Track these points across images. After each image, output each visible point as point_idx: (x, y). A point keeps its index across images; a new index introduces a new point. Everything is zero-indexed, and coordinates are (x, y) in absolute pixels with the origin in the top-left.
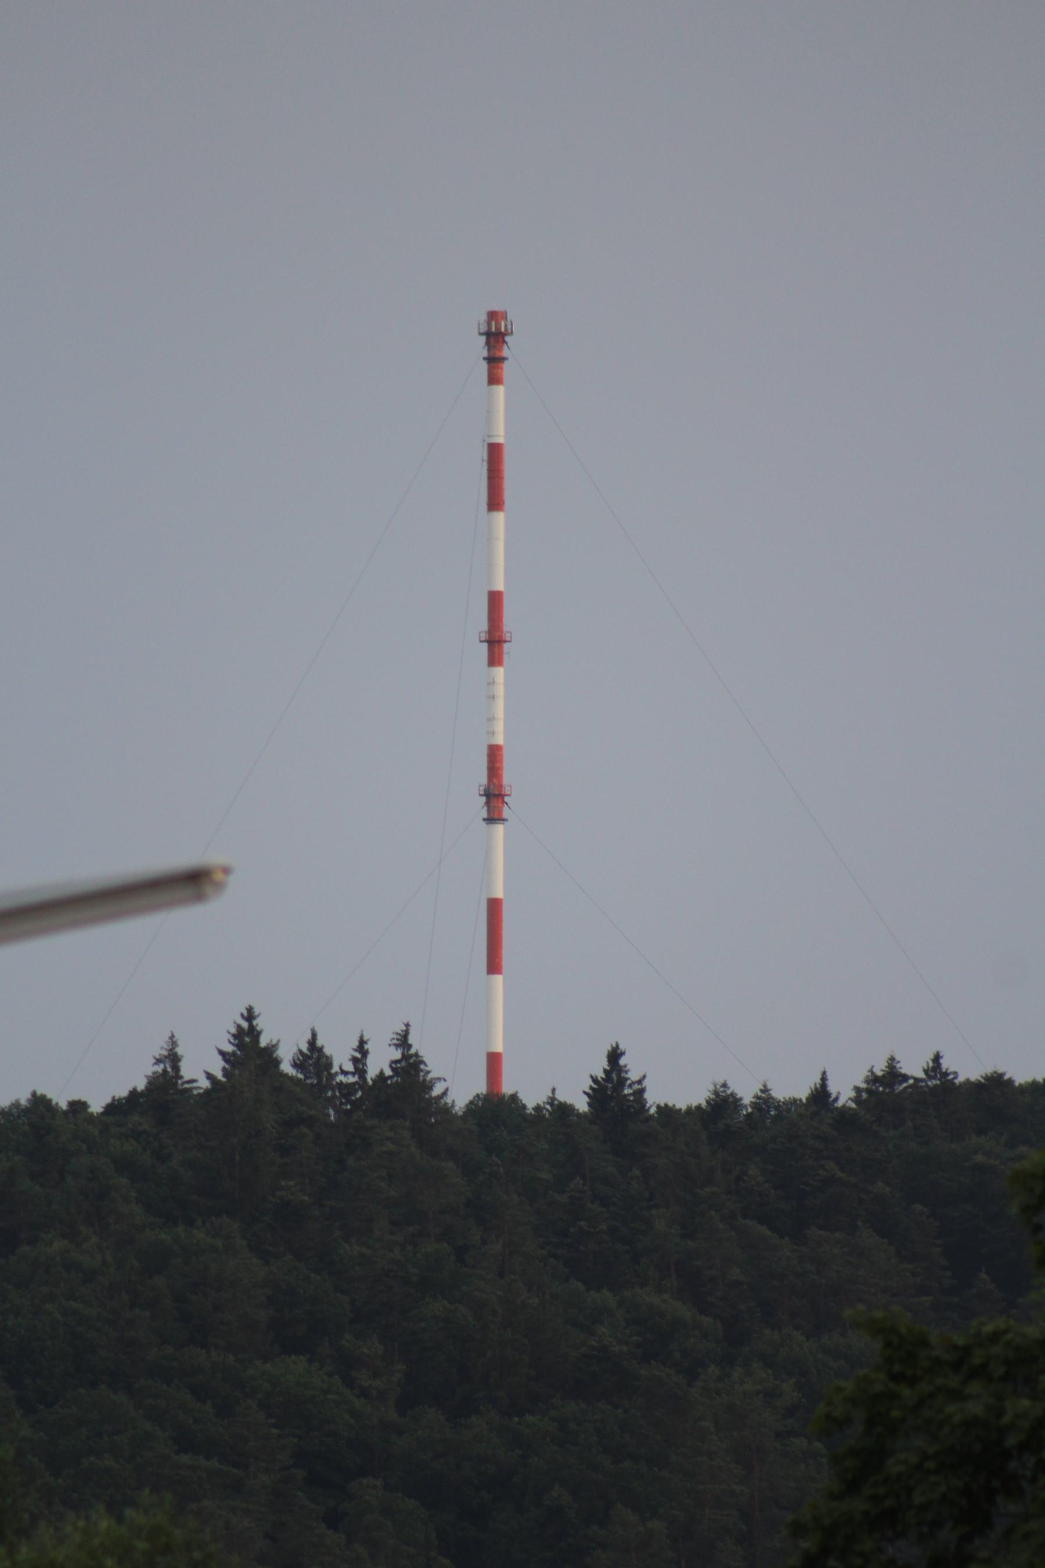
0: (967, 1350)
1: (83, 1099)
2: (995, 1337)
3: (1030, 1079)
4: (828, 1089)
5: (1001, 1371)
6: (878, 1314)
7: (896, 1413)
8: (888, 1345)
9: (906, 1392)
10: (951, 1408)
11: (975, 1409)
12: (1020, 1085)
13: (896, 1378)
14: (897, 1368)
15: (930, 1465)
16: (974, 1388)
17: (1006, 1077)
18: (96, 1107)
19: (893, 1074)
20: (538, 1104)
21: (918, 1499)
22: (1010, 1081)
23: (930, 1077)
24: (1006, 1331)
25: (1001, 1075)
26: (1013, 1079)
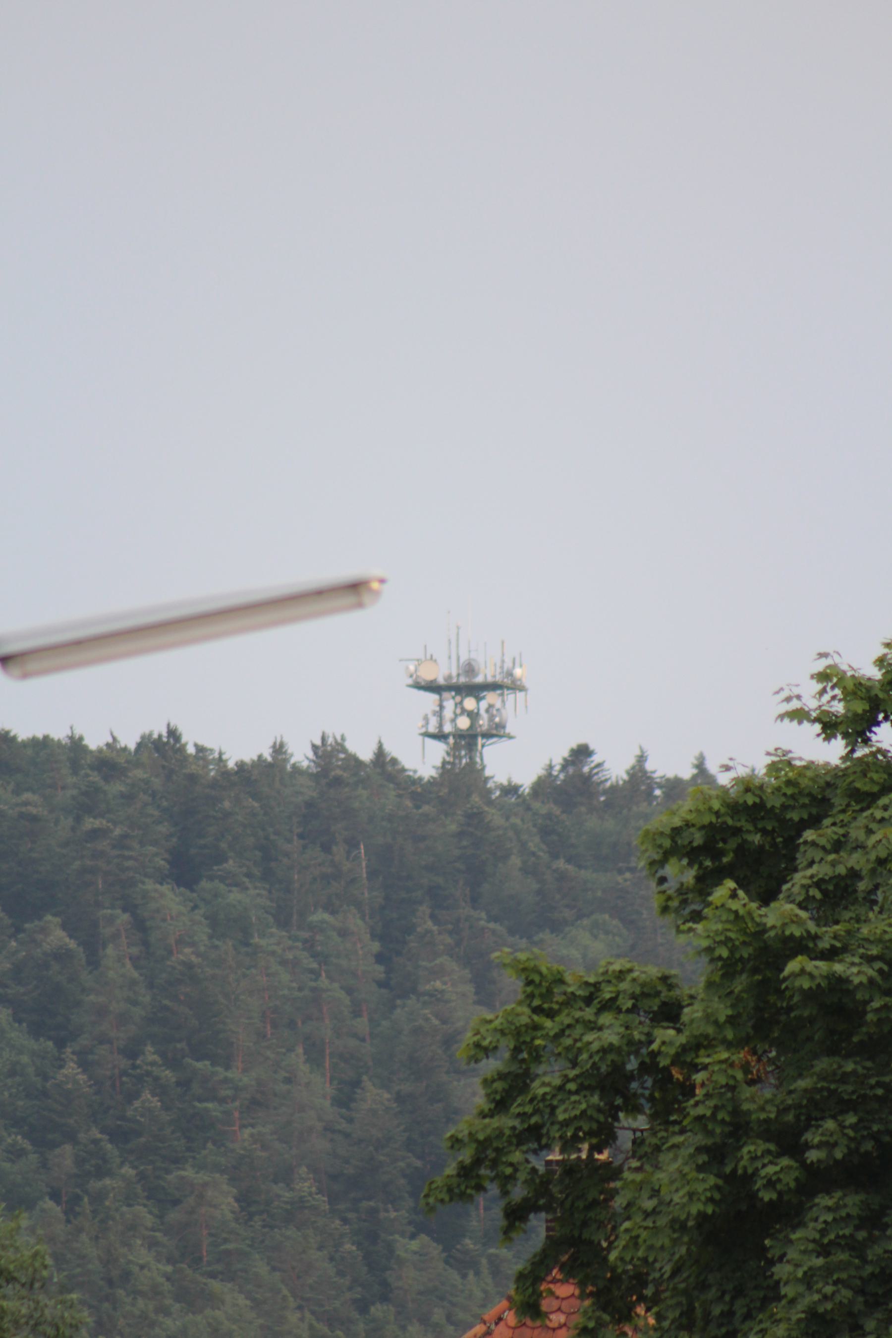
0: (596, 986)
1: (574, 745)
2: (621, 975)
3: (30, 736)
4: (350, 751)
5: (629, 1004)
6: (522, 956)
7: (538, 1042)
8: (529, 983)
9: (548, 1023)
10: (589, 1037)
11: (611, 1037)
12: (23, 741)
13: (537, 1010)
14: (536, 1002)
15: (572, 1086)
16: (606, 1019)
17: (12, 734)
18: (20, 740)
19: (144, 734)
20: (260, 757)
21: (561, 1117)
22: (14, 738)
23: (844, 762)
24: (630, 971)
25: (7, 733)
26: (17, 736)
